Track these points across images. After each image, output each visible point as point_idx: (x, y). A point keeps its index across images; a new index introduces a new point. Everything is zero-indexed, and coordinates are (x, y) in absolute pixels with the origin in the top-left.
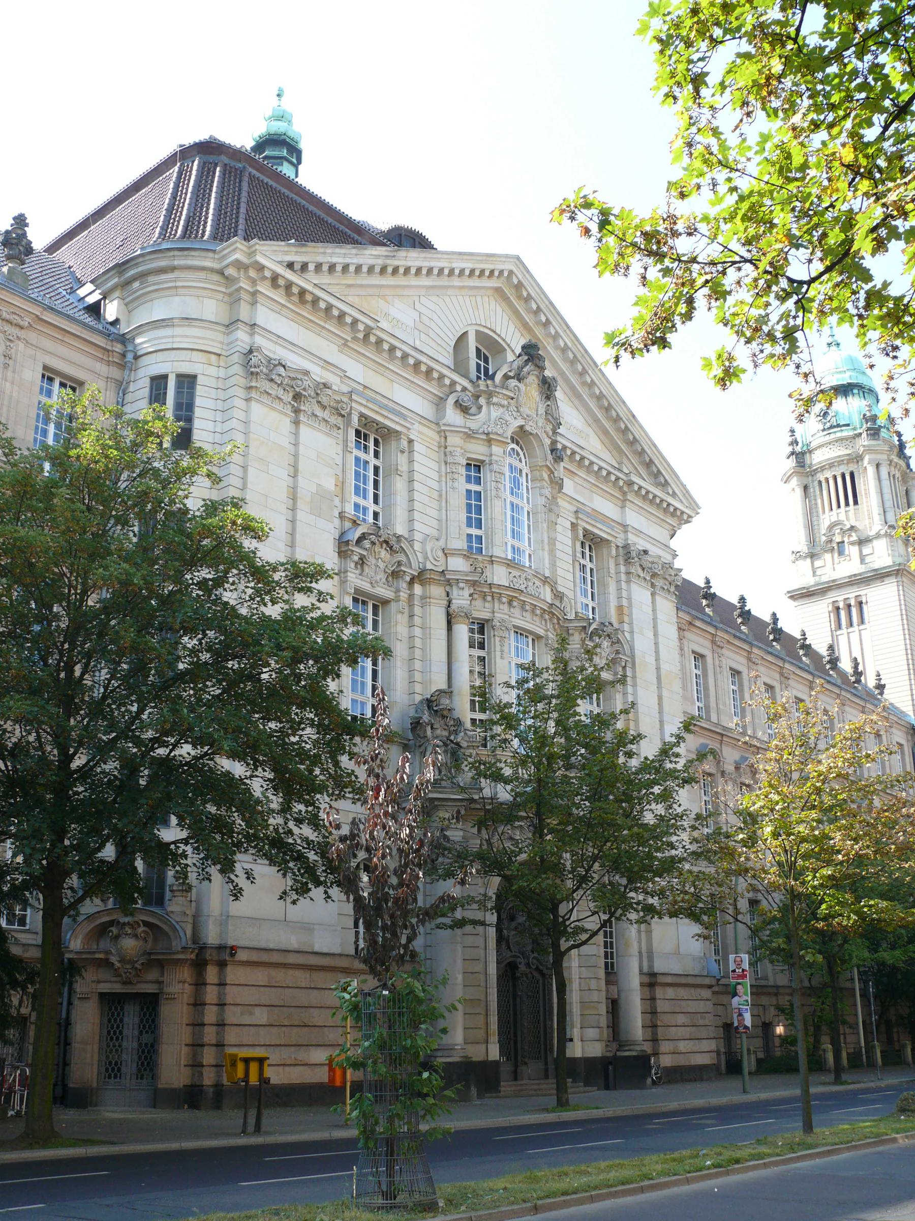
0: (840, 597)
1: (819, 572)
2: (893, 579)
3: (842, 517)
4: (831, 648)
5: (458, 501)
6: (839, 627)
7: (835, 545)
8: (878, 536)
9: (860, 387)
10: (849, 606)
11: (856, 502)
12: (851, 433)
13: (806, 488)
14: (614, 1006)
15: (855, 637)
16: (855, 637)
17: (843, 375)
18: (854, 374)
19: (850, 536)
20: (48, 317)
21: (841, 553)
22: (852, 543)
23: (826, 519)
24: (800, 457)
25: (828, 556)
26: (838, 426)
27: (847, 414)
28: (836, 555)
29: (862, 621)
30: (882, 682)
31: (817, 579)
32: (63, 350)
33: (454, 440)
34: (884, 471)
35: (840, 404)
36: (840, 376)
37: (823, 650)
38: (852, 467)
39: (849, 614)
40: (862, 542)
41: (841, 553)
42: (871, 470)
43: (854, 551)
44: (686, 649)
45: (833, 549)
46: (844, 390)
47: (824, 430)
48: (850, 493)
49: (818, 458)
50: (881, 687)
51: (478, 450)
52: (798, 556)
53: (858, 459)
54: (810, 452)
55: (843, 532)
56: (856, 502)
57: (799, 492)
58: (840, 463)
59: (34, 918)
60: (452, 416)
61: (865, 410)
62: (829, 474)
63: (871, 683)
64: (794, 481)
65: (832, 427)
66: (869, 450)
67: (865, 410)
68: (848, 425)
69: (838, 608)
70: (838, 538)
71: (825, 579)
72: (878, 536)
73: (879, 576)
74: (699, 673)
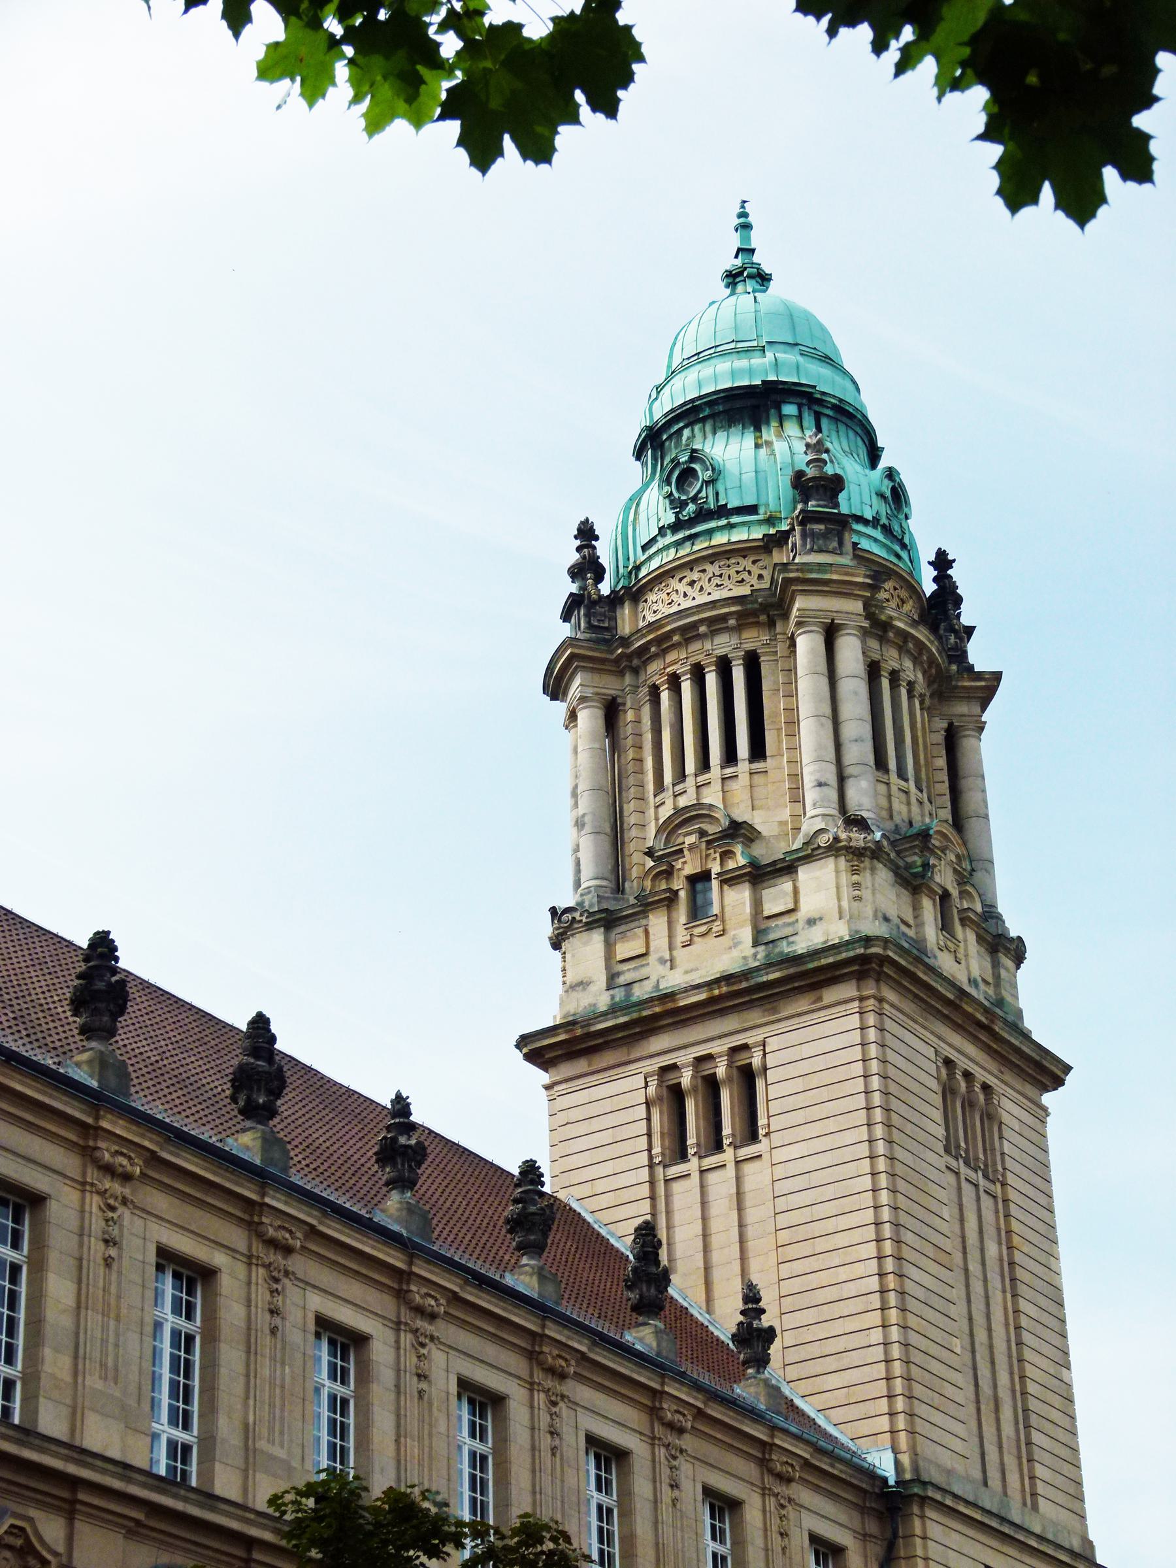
0: (679, 1048)
2: (847, 990)
3: (712, 796)
4: (647, 1235)
7: (679, 884)
9: (807, 399)
10: (712, 1085)
11: (758, 751)
12: (758, 533)
13: (612, 712)
16: (722, 1184)
17: (757, 361)
18: (789, 357)
19: (726, 855)
20: (715, 1411)
21: (697, 912)
26: (723, 511)
27: (749, 477)
30: (766, 1321)
31: (619, 994)
32: (491, 1351)
35: (730, 451)
36: (742, 363)
37: (623, 1240)
38: (753, 639)
39: (711, 1113)
42: (808, 645)
44: (567, 1431)
45: (671, 899)
46: (749, 406)
47: (676, 527)
50: (755, 1339)
56: (758, 751)
58: (717, 625)
61: (802, 459)
62: (679, 661)
63: (725, 1321)
65: (703, 515)
67: (802, 459)
68: (752, 509)
69: (677, 1095)
71: (641, 992)
73: (791, 980)
74: (722, 1550)
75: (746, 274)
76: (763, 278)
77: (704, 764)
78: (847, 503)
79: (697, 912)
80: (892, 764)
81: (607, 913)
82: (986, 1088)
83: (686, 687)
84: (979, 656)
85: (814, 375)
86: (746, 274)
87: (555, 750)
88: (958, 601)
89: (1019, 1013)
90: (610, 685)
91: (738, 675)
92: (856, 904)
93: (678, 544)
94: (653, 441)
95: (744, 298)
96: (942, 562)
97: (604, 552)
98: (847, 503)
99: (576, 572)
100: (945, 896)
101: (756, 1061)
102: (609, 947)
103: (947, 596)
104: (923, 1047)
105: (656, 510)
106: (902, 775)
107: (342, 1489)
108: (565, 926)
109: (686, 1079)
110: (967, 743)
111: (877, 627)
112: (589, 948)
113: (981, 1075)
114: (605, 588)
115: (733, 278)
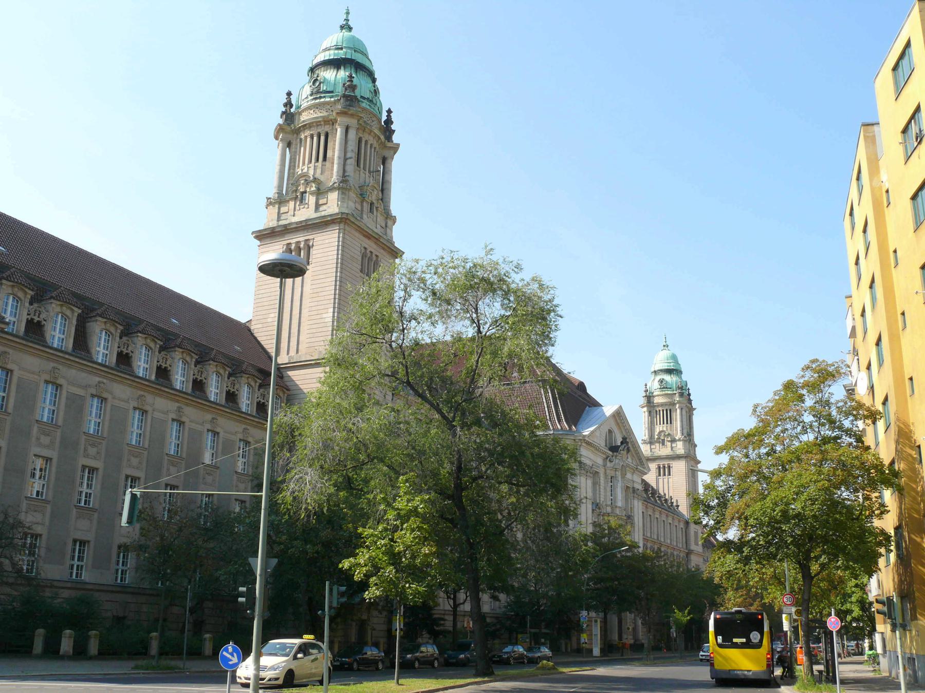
0: (661, 463)
1: (283, 217)
5: (609, 489)
6: (660, 475)
8: (679, 440)
10: (300, 249)
13: (650, 412)
14: (635, 629)
15: (666, 480)
16: (666, 480)
21: (663, 444)
22: (312, 193)
23: (658, 429)
24: (649, 398)
25: (657, 445)
28: (298, 203)
29: (669, 474)
33: (608, 471)
34: (352, 134)
35: (329, 75)
38: (327, 128)
39: (665, 471)
40: (673, 441)
41: (663, 444)
42: (339, 132)
43: (669, 444)
46: (669, 371)
48: (670, 421)
49: (657, 400)
50: (678, 506)
51: (613, 473)
52: (270, 203)
53: (674, 404)
54: (300, 114)
55: (665, 436)
57: (647, 413)
59: (486, 608)
60: (609, 464)
62: (307, 133)
64: (645, 409)
66: (679, 402)
68: (332, 92)
70: (302, 189)
71: (656, 454)
72: (679, 440)
73: (678, 457)
75: (346, 27)
76: (350, 29)
77: (317, 160)
78: (358, 93)
79: (301, 201)
80: (362, 166)
81: (280, 201)
82: (377, 256)
83: (315, 138)
84: (396, 138)
85: (359, 58)
86: (346, 27)
87: (271, 153)
88: (392, 123)
89: (392, 237)
90: (290, 137)
91: (323, 138)
92: (849, 294)
93: (316, 99)
94: (312, 70)
95: (346, 33)
96: (389, 112)
97: (294, 99)
98: (358, 93)
99: (285, 105)
100: (372, 204)
101: (311, 244)
102: (279, 209)
103: (389, 121)
104: (359, 243)
105: (307, 90)
106: (364, 169)
107: (414, 557)
108: (270, 203)
109: (293, 247)
110: (388, 161)
111: (362, 128)
112: (274, 210)
113: (375, 252)
114: (293, 110)
115: (342, 27)
